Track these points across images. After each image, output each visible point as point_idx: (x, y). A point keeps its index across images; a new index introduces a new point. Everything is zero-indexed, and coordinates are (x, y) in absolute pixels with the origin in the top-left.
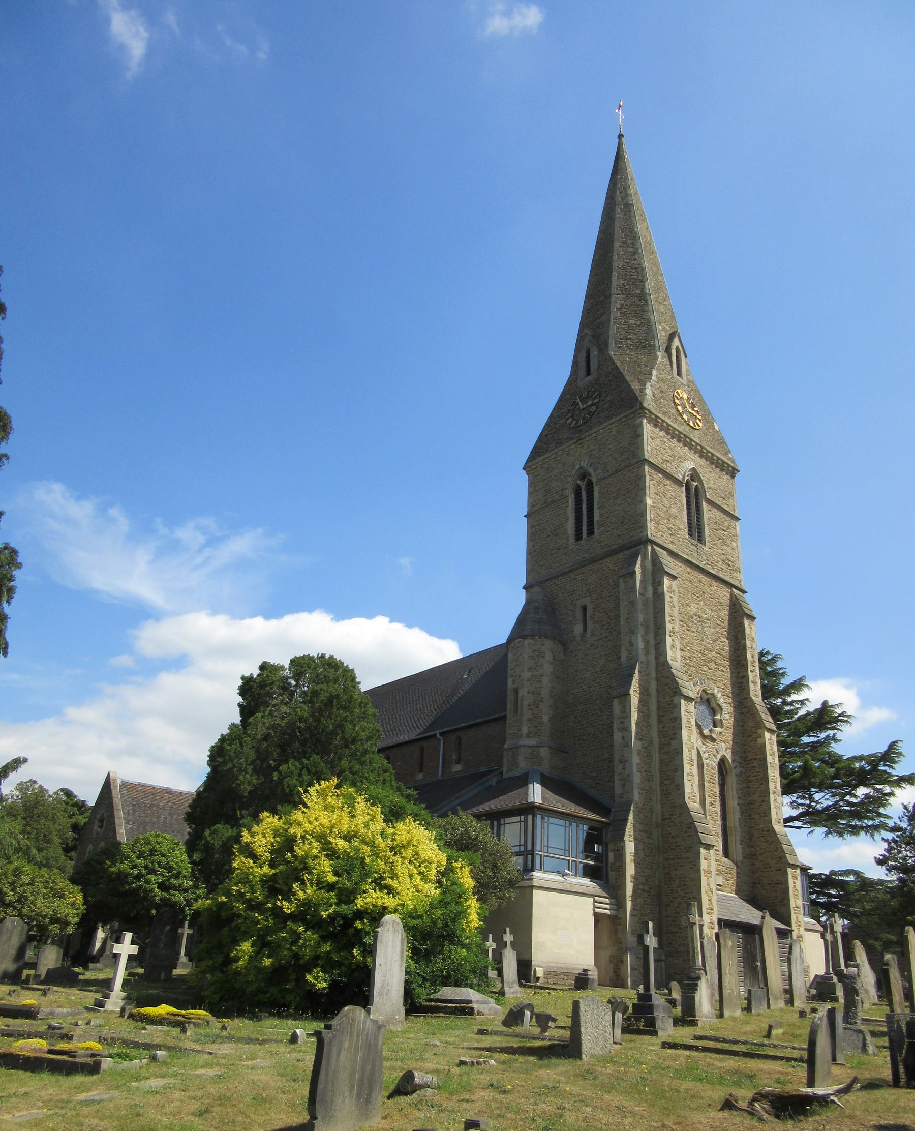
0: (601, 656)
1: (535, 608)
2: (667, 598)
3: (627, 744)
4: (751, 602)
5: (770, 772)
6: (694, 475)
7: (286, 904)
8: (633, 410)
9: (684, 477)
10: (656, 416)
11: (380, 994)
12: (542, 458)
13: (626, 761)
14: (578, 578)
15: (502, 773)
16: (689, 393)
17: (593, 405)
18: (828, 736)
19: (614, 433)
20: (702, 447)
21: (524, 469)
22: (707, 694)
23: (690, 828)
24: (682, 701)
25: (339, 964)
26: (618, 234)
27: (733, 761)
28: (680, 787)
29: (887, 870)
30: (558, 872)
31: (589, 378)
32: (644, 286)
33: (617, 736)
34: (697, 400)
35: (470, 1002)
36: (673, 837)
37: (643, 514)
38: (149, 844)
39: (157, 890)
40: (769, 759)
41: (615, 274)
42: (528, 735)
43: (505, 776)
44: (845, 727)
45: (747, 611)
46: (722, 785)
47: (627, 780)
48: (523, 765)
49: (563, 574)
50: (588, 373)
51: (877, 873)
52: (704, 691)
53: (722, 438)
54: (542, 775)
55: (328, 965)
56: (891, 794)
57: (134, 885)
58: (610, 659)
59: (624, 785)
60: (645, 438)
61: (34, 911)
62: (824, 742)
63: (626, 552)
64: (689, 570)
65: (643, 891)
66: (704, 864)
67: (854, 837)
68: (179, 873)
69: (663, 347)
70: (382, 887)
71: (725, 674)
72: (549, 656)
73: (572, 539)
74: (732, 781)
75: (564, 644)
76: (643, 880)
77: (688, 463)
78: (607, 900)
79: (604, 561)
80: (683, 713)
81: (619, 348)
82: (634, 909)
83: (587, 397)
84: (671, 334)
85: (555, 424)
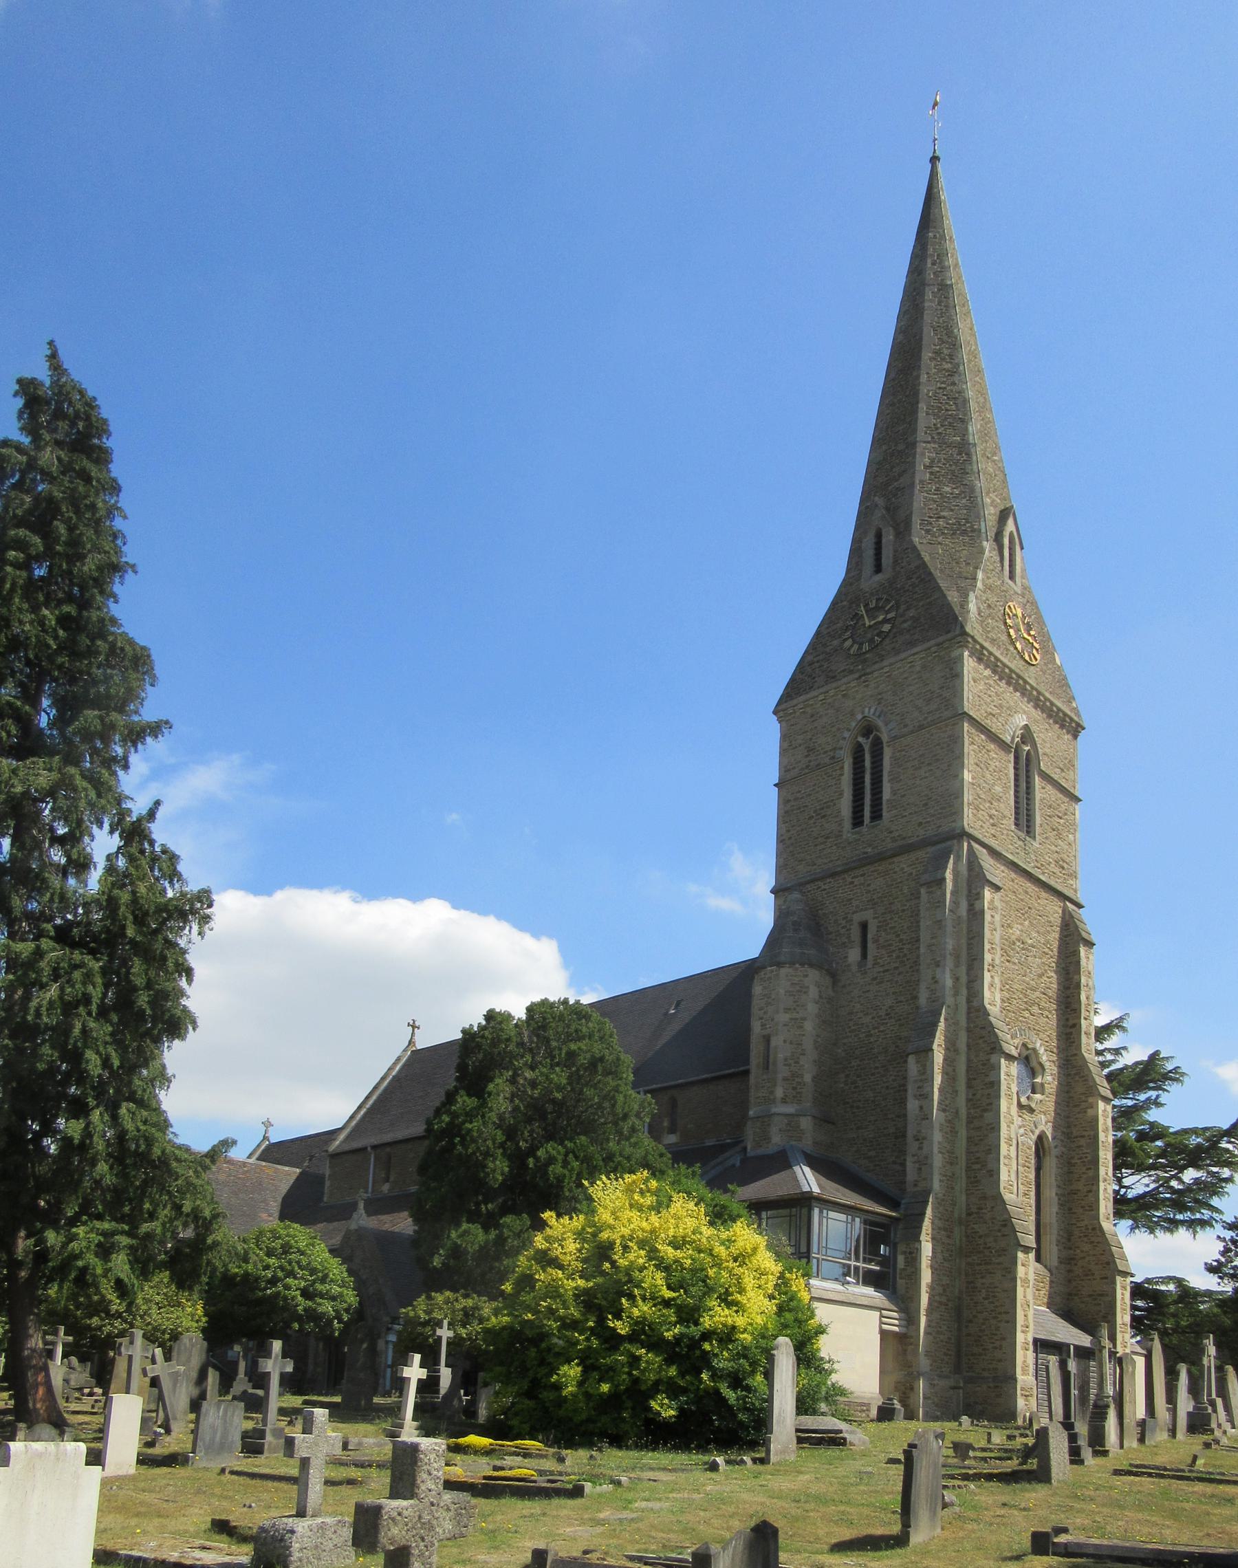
0: (887, 995)
1: (794, 923)
2: (987, 917)
3: (926, 1116)
4: (1090, 920)
5: (1101, 1154)
6: (1027, 735)
7: (618, 1324)
8: (949, 636)
9: (1013, 738)
10: (982, 647)
11: (778, 1422)
13: (924, 1138)
14: (856, 881)
15: (745, 1149)
16: (1024, 607)
17: (885, 621)
18: (1149, 1099)
19: (918, 668)
20: (1039, 693)
21: (775, 713)
22: (1028, 1049)
23: (1005, 1225)
24: (1002, 1060)
25: (684, 1391)
26: (929, 337)
27: (1054, 1138)
28: (994, 1174)
29: (1220, 1278)
30: (836, 1280)
31: (879, 577)
32: (967, 429)
33: (912, 1105)
34: (1035, 621)
35: (841, 1432)
36: (980, 1237)
37: (959, 794)
38: (279, 1238)
39: (300, 1298)
40: (1102, 1136)
41: (922, 406)
42: (782, 1101)
43: (750, 1153)
44: (1173, 1088)
45: (1084, 934)
46: (1038, 1169)
47: (924, 1163)
48: (777, 1140)
50: (878, 568)
51: (1209, 1283)
52: (1024, 1045)
53: (1065, 678)
54: (805, 1153)
55: (674, 1391)
56: (1229, 1180)
57: (269, 1291)
58: (902, 998)
59: (920, 1169)
60: (966, 680)
61: (149, 1324)
62: (1142, 1107)
63: (930, 849)
64: (1013, 875)
65: (940, 1303)
66: (1021, 1271)
67: (1168, 1234)
68: (326, 1276)
69: (991, 534)
70: (729, 1304)
71: (1049, 1022)
72: (813, 992)
73: (847, 824)
74: (1051, 1164)
75: (833, 976)
76: (940, 1290)
77: (1020, 717)
78: (895, 1315)
79: (895, 859)
80: (1003, 1077)
82: (928, 1326)
83: (877, 608)
84: (1001, 512)
85: (825, 645)
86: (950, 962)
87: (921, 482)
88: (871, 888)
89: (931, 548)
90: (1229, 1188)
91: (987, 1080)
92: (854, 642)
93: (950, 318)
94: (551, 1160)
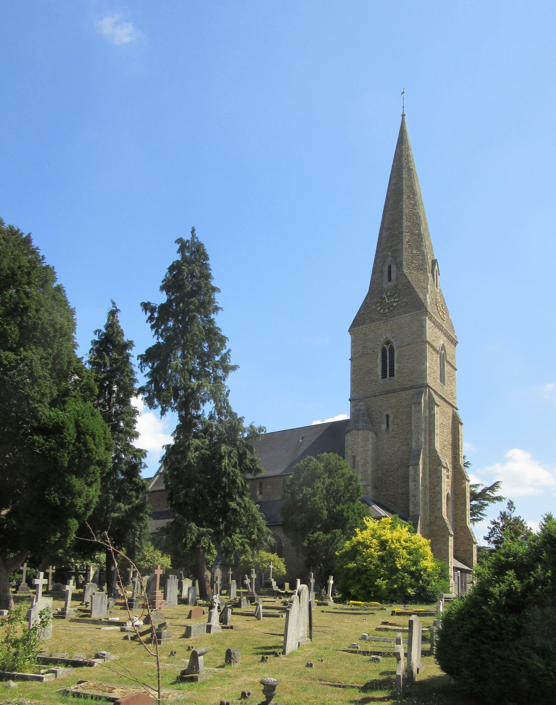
1: (363, 414)
3: (417, 489)
6: (443, 348)
8: (421, 311)
12: (361, 327)
17: (394, 302)
33: (411, 484)
47: (416, 505)
49: (375, 396)
50: (390, 280)
55: (412, 587)
56: (487, 505)
59: (415, 507)
72: (371, 440)
73: (380, 377)
75: (376, 433)
79: (400, 393)
81: (409, 268)
86: (423, 433)
87: (406, 248)
88: (390, 402)
89: (411, 275)
90: (486, 507)
91: (437, 475)
92: (382, 308)
93: (412, 182)
94: (342, 511)
